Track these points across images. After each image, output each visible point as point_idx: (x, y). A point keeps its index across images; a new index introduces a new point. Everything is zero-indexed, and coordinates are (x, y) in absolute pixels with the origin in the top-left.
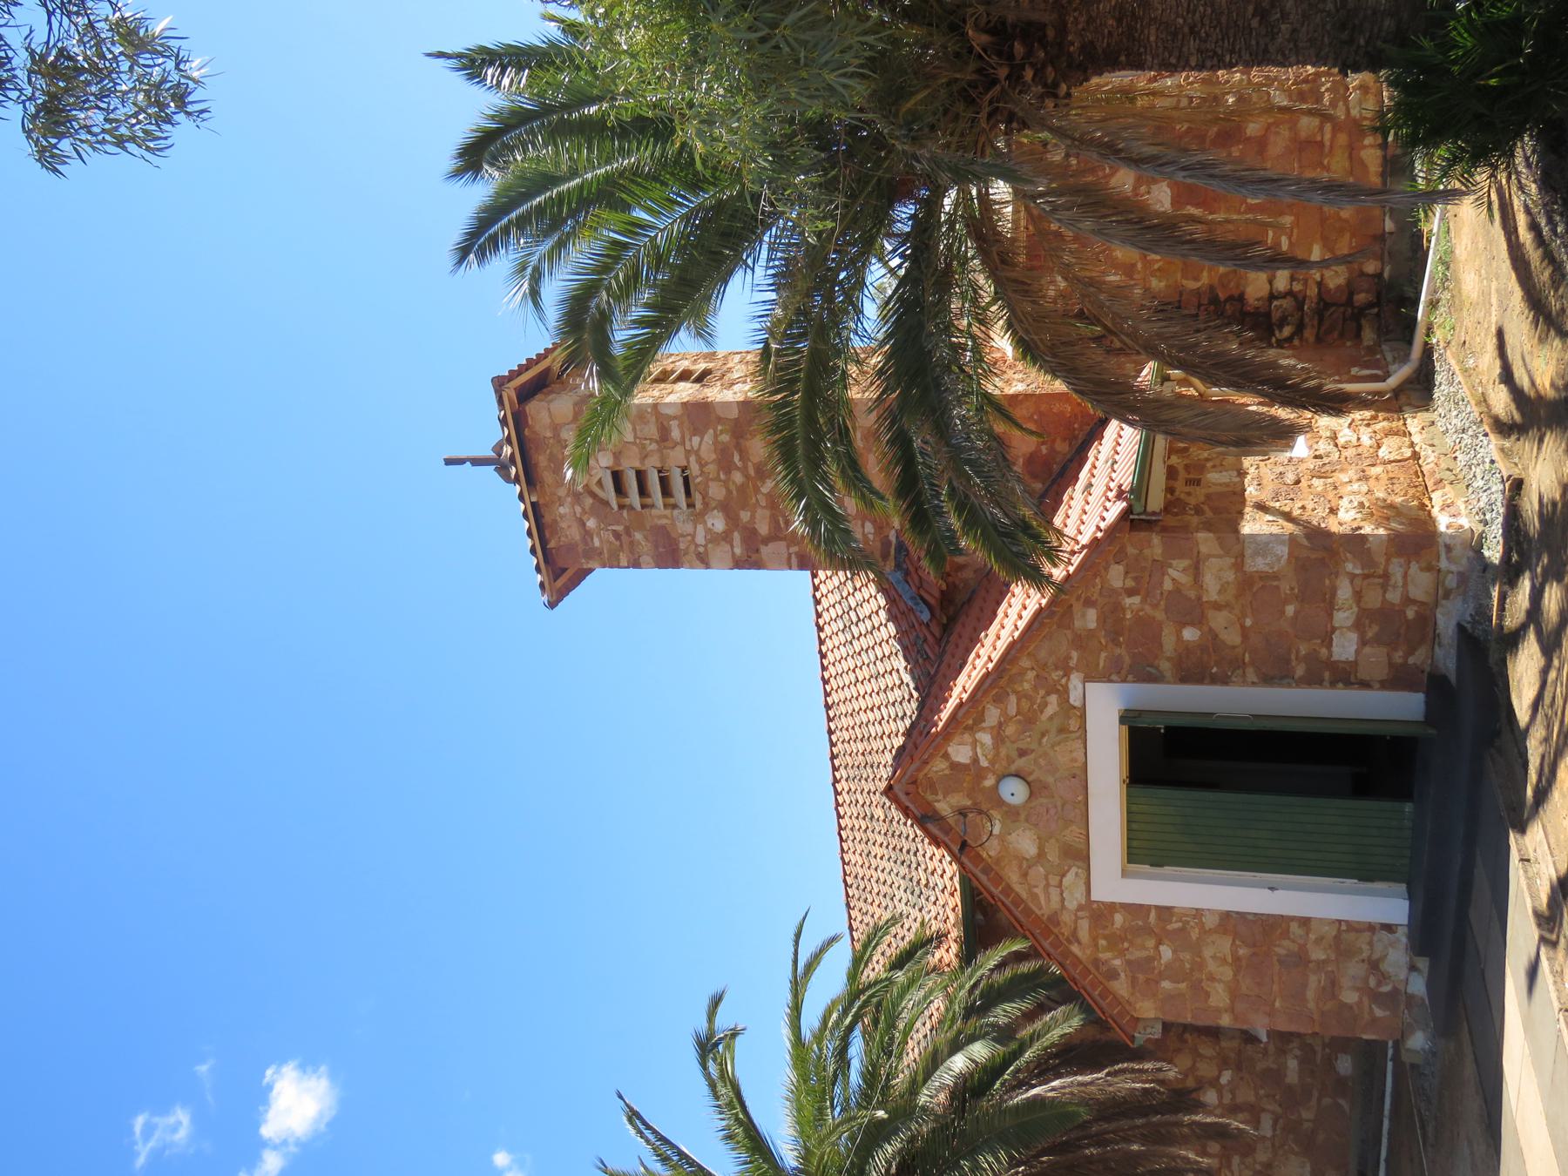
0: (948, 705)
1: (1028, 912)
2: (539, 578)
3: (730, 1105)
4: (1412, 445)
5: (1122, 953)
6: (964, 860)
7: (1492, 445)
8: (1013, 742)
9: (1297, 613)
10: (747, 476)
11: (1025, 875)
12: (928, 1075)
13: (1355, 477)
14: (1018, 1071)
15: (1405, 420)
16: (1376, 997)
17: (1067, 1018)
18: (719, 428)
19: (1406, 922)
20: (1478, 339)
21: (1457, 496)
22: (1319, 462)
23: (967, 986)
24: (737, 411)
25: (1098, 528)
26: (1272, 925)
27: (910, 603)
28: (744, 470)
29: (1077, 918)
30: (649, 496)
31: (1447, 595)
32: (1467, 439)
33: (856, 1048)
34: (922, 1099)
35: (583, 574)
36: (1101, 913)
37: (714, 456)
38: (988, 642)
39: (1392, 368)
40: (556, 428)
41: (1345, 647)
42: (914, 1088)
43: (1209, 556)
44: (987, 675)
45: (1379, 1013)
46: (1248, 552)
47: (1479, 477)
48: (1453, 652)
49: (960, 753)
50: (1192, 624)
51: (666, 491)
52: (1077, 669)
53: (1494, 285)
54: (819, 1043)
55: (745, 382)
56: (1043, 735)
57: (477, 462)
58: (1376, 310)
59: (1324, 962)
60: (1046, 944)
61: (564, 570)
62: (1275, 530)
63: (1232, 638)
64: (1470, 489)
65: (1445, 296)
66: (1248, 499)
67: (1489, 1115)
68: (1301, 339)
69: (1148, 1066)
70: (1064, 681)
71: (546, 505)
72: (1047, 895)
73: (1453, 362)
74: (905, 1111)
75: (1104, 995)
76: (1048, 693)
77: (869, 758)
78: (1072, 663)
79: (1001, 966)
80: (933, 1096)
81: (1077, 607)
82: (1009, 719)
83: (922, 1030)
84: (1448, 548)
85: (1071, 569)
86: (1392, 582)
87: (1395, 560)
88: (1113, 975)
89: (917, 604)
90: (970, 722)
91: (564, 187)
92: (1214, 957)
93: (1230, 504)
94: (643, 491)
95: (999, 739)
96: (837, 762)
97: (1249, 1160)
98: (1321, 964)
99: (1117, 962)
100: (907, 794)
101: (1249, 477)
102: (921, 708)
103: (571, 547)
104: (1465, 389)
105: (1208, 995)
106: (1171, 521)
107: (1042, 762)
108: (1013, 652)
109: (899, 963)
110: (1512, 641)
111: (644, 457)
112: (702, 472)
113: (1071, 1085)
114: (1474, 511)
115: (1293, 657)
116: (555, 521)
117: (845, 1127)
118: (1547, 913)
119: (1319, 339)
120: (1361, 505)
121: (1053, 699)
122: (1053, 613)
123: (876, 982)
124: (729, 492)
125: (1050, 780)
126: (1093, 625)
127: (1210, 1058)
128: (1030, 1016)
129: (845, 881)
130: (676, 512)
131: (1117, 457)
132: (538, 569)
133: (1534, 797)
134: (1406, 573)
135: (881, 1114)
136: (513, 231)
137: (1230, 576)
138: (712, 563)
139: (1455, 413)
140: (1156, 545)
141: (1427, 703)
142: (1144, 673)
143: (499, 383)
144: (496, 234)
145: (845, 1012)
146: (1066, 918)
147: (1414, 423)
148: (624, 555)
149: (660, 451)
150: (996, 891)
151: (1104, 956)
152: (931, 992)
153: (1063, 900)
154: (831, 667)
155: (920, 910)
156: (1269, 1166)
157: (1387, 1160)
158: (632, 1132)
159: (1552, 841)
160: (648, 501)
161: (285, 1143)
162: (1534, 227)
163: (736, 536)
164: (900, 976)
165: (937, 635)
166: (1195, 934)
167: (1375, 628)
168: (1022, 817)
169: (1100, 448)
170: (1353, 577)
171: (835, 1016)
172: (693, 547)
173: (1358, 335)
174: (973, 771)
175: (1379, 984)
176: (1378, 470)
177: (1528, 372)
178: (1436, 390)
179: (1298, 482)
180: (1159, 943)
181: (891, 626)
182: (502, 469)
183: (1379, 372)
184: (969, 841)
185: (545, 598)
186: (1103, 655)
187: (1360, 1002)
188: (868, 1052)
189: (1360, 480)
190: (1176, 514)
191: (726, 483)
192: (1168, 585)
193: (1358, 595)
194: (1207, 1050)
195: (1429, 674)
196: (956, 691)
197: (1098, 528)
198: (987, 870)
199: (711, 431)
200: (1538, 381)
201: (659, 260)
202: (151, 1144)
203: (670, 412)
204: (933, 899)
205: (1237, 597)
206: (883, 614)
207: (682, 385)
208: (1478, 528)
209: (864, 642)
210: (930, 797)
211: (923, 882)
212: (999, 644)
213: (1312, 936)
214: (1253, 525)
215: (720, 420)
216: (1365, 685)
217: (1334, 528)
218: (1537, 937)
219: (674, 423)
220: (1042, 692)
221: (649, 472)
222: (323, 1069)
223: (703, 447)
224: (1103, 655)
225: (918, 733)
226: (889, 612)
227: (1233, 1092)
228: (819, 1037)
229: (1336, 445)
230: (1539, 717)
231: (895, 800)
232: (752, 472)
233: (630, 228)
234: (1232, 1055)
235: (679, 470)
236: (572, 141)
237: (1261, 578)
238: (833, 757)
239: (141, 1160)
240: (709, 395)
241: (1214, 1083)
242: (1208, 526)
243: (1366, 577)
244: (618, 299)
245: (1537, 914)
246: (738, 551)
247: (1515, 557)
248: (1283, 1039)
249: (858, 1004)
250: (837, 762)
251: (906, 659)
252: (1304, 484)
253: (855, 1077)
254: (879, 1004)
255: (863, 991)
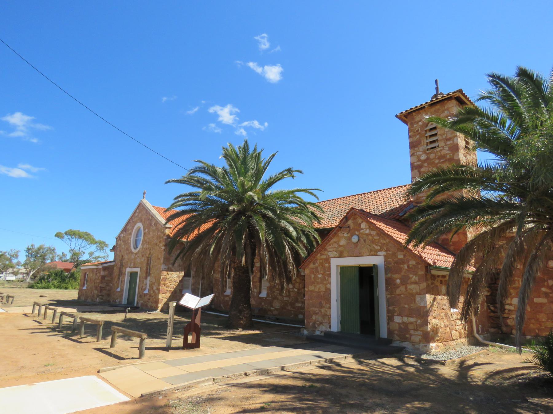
0: (375, 222)
1: (327, 244)
2: (404, 112)
3: (277, 178)
4: (457, 339)
5: (319, 266)
6: (337, 228)
7: (457, 360)
8: (367, 238)
9: (405, 308)
10: (437, 164)
11: (335, 242)
12: (288, 222)
13: (445, 324)
14: (291, 242)
15: (465, 338)
16: (314, 324)
17: (304, 253)
18: (451, 155)
19: (332, 331)
20: (489, 358)
21: (441, 350)
22: (450, 315)
23: (309, 230)
24: (456, 159)
25: (425, 258)
26: (328, 300)
27: (404, 210)
28: (439, 163)
29: (326, 255)
30: (430, 138)
31: (413, 345)
32: (458, 353)
33: (293, 205)
34: (283, 221)
35: (406, 123)
36: (328, 260)
37: (442, 154)
38: (393, 231)
39: (482, 336)
40: (448, 109)
41: (397, 319)
42: (286, 219)
43: (419, 286)
44: (384, 231)
45: (311, 324)
46: (421, 296)
47: (447, 355)
48: (398, 345)
49: (363, 225)
50: (401, 282)
51: (431, 142)
52: (387, 253)
53: (506, 363)
54: (293, 197)
55: (466, 160)
56: (369, 246)
57: (437, 89)
58: (500, 332)
59: (321, 312)
60: (319, 248)
61: (407, 118)
62: (428, 303)
63: (398, 291)
64: (443, 353)
65: (504, 351)
66: (437, 296)
67: (289, 346)
68: (490, 312)
69: (295, 272)
70: (384, 250)
71: (425, 110)
72: (331, 248)
73: (482, 351)
74: (280, 217)
75: (309, 262)
76: (380, 246)
77: (364, 203)
78: (388, 252)
79: (314, 238)
80: (283, 223)
81: (403, 253)
82: (373, 237)
83: (300, 221)
84: (426, 346)
85: (413, 251)
86: (416, 331)
87: (421, 333)
88: (314, 264)
89: (404, 212)
90: (371, 227)
91: (517, 101)
92: (320, 287)
93: (435, 292)
94: (431, 136)
95: (368, 235)
96: (363, 195)
97: (279, 295)
98: (320, 311)
99: (317, 265)
100: (352, 213)
101: (444, 297)
102: (375, 215)
103: (413, 119)
104: (474, 354)
105: (311, 285)
106: (429, 276)
107: (363, 245)
108: (390, 237)
109: (313, 213)
110: (401, 359)
111: (441, 135)
112: (438, 151)
113: (289, 255)
114: (437, 353)
115: (394, 307)
116: (420, 113)
117: (275, 204)
118: (333, 361)
119: (490, 317)
120: (437, 325)
121: (379, 248)
122: (401, 247)
123: (308, 209)
124: (433, 159)
125: (359, 247)
126: (399, 257)
127: (299, 286)
128: (304, 245)
129: (334, 199)
130: (425, 146)
131: (448, 262)
132: (406, 111)
133: (362, 361)
134: (418, 335)
135: (278, 212)
136: (502, 89)
137: (414, 291)
138: (412, 157)
139: (467, 351)
140: (422, 272)
141: (384, 339)
142: (387, 270)
143: (460, 91)
144: (500, 84)
145: (301, 202)
146: (326, 253)
147: (464, 340)
148: (412, 133)
149: (443, 139)
150: (331, 236)
151: (318, 261)
152: (308, 222)
153: (330, 252)
154: (387, 191)
155: (327, 218)
156: (278, 299)
157: (281, 325)
158: (270, 156)
159: (350, 364)
160: (428, 138)
161: (264, 72)
162: (523, 374)
163: (419, 163)
164: (310, 214)
165: (396, 218)
166: (325, 282)
167: (403, 327)
168: (349, 241)
169: (452, 258)
170: (416, 322)
171: (299, 200)
172: (415, 151)
173: (492, 327)
174: (359, 229)
175: (317, 324)
176: (448, 329)
177: (477, 369)
178: (474, 347)
179: (443, 309)
180: (322, 274)
181: (399, 206)
182: (435, 96)
183: (480, 332)
184: (342, 229)
185: (398, 114)
186: (391, 260)
187: (313, 320)
188: (292, 208)
189: (445, 325)
190: (431, 278)
191: (435, 158)
192: (411, 276)
193: (411, 323)
194: (301, 286)
195: (392, 339)
196: (379, 224)
197: (425, 258)
198: (335, 233)
199: (450, 152)
200: (473, 371)
201: (494, 132)
202: (260, 39)
203: (455, 140)
204: (330, 221)
205: (409, 293)
206: (401, 203)
207: (464, 142)
208: (432, 354)
209: (394, 199)
210: (352, 219)
211: (334, 218)
212: (393, 233)
213: (327, 309)
214: (429, 298)
215: (454, 154)
216: (388, 324)
217: (429, 318)
218: (327, 358)
219: (451, 142)
220: (380, 245)
221: (436, 137)
222: (282, 78)
223: (445, 151)
224: (391, 260)
225: (369, 215)
226: (402, 205)
227: (292, 291)
228: (295, 197)
229: (455, 320)
230: (380, 364)
231: (350, 211)
232: (439, 165)
233: (502, 123)
234: (300, 291)
235: (438, 145)
236: (531, 101)
237: (414, 299)
238: (364, 194)
239: (256, 38)
240: (461, 150)
241: (294, 287)
242: (428, 286)
243: (417, 325)
244: (479, 123)
245: (332, 359)
246: (416, 164)
247: (423, 362)
248: (303, 303)
249: (303, 205)
250: (363, 195)
251: (389, 210)
252: (443, 311)
253: (286, 206)
254: (303, 210)
255: (304, 205)
